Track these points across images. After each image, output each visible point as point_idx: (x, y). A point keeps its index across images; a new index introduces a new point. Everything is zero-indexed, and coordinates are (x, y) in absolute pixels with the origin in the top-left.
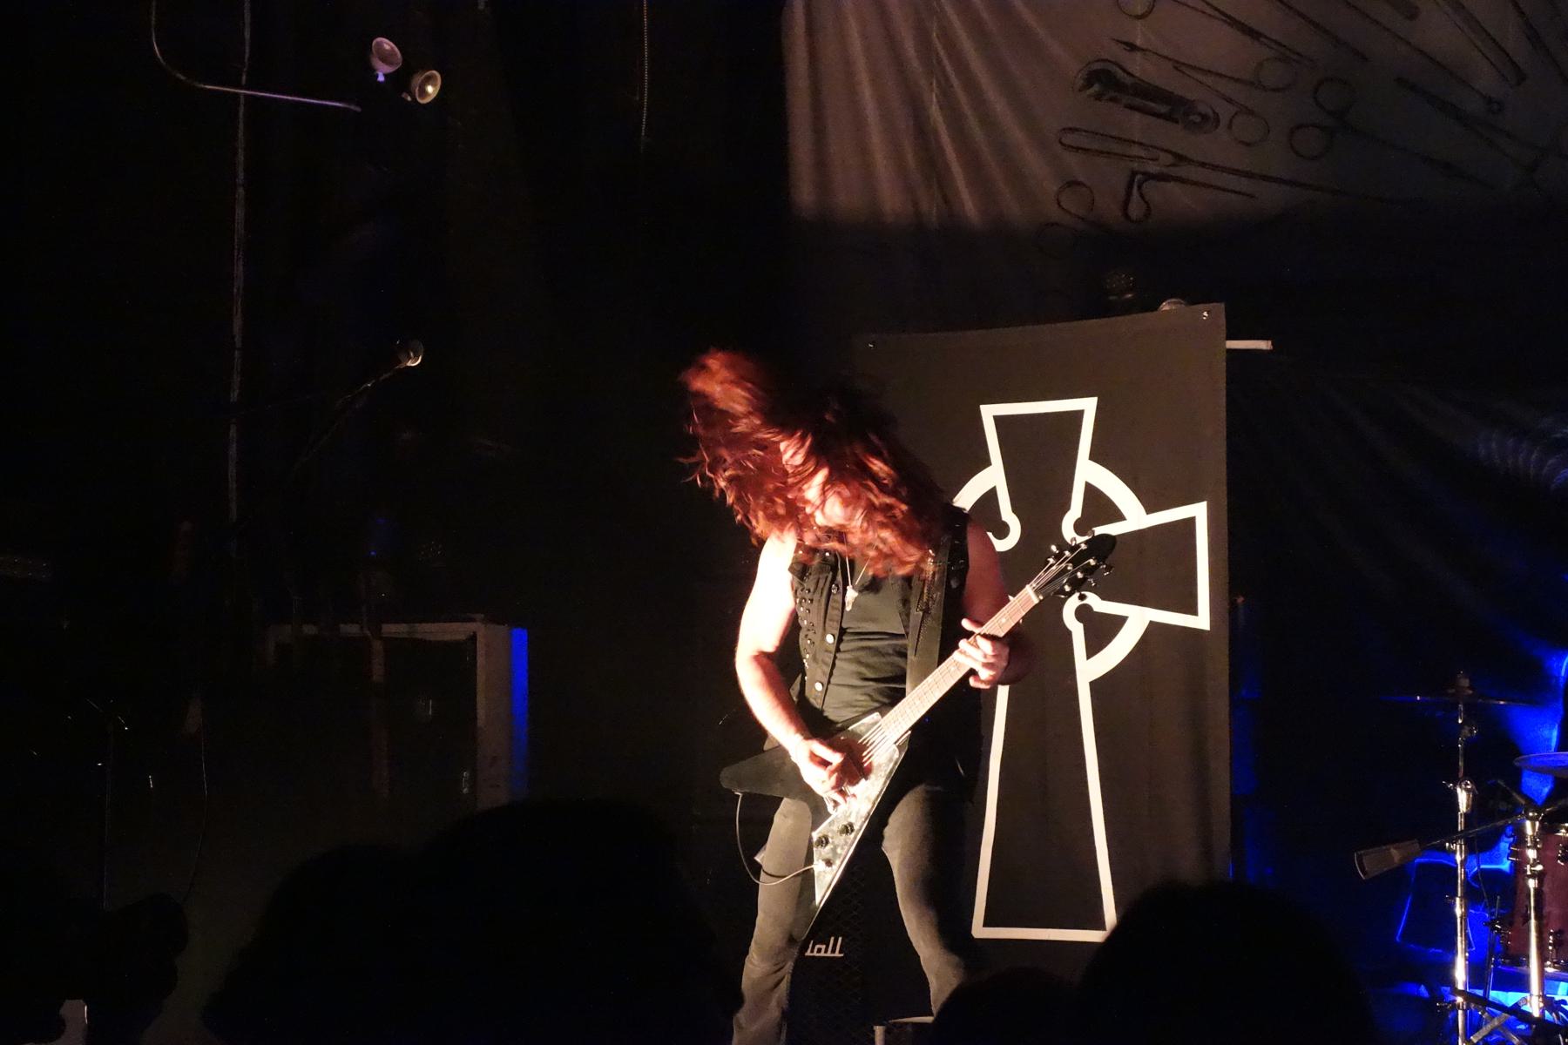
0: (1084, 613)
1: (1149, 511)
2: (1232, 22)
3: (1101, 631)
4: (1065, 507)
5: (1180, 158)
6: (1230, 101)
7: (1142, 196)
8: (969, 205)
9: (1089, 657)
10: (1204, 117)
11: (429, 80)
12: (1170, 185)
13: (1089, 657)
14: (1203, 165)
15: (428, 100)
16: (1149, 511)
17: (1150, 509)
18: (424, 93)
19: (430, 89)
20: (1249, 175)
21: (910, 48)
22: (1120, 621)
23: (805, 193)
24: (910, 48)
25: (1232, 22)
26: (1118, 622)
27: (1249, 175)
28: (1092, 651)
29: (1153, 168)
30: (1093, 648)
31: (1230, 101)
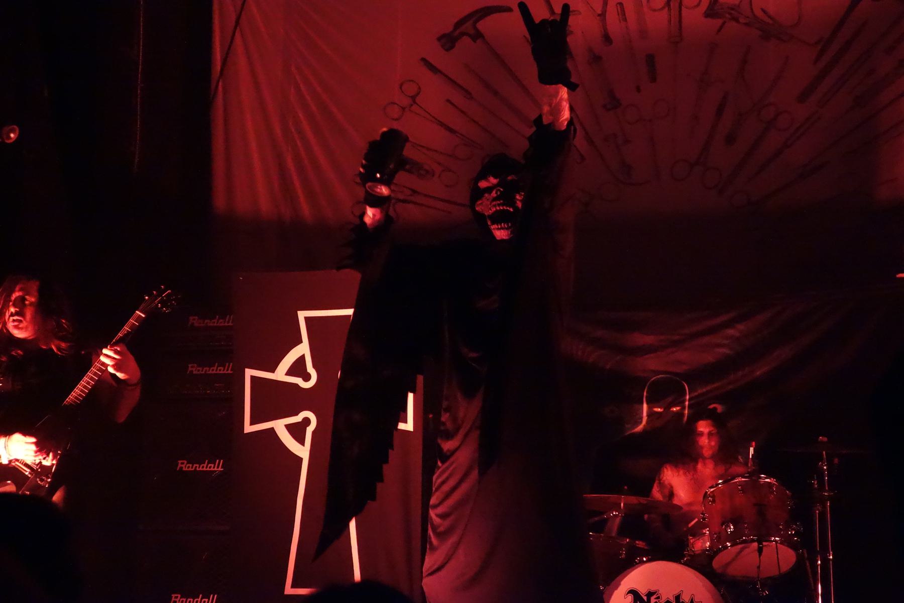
0: (307, 377)
1: (273, 428)
2: (442, 124)
3: (298, 368)
4: (314, 433)
5: (414, 192)
6: (439, 164)
7: (395, 211)
8: (306, 210)
9: (303, 356)
10: (427, 171)
11: (13, 131)
12: (410, 206)
13: (303, 356)
14: (426, 196)
15: (11, 141)
16: (273, 428)
17: (272, 431)
18: (9, 138)
19: (12, 135)
20: (442, 200)
21: (278, 131)
22: (289, 373)
23: (220, 201)
24: (278, 131)
25: (442, 124)
26: (289, 373)
27: (442, 200)
28: (302, 358)
29: (401, 197)
30: (302, 359)
31: (439, 164)
